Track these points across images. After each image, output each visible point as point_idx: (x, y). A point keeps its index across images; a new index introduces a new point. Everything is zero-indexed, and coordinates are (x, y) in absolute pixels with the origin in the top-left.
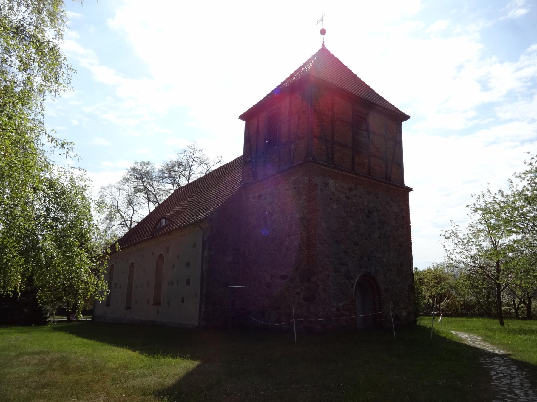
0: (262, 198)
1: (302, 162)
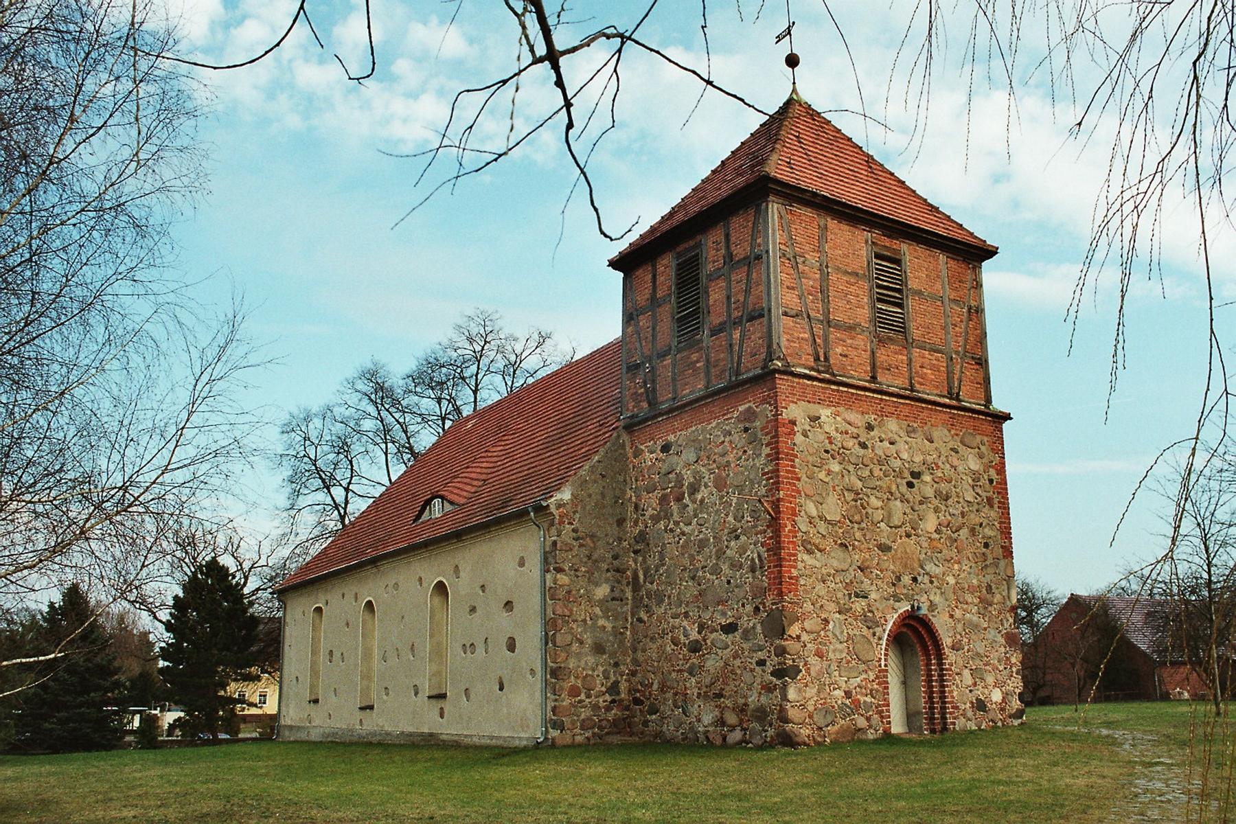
0: (671, 452)
1: (759, 371)
